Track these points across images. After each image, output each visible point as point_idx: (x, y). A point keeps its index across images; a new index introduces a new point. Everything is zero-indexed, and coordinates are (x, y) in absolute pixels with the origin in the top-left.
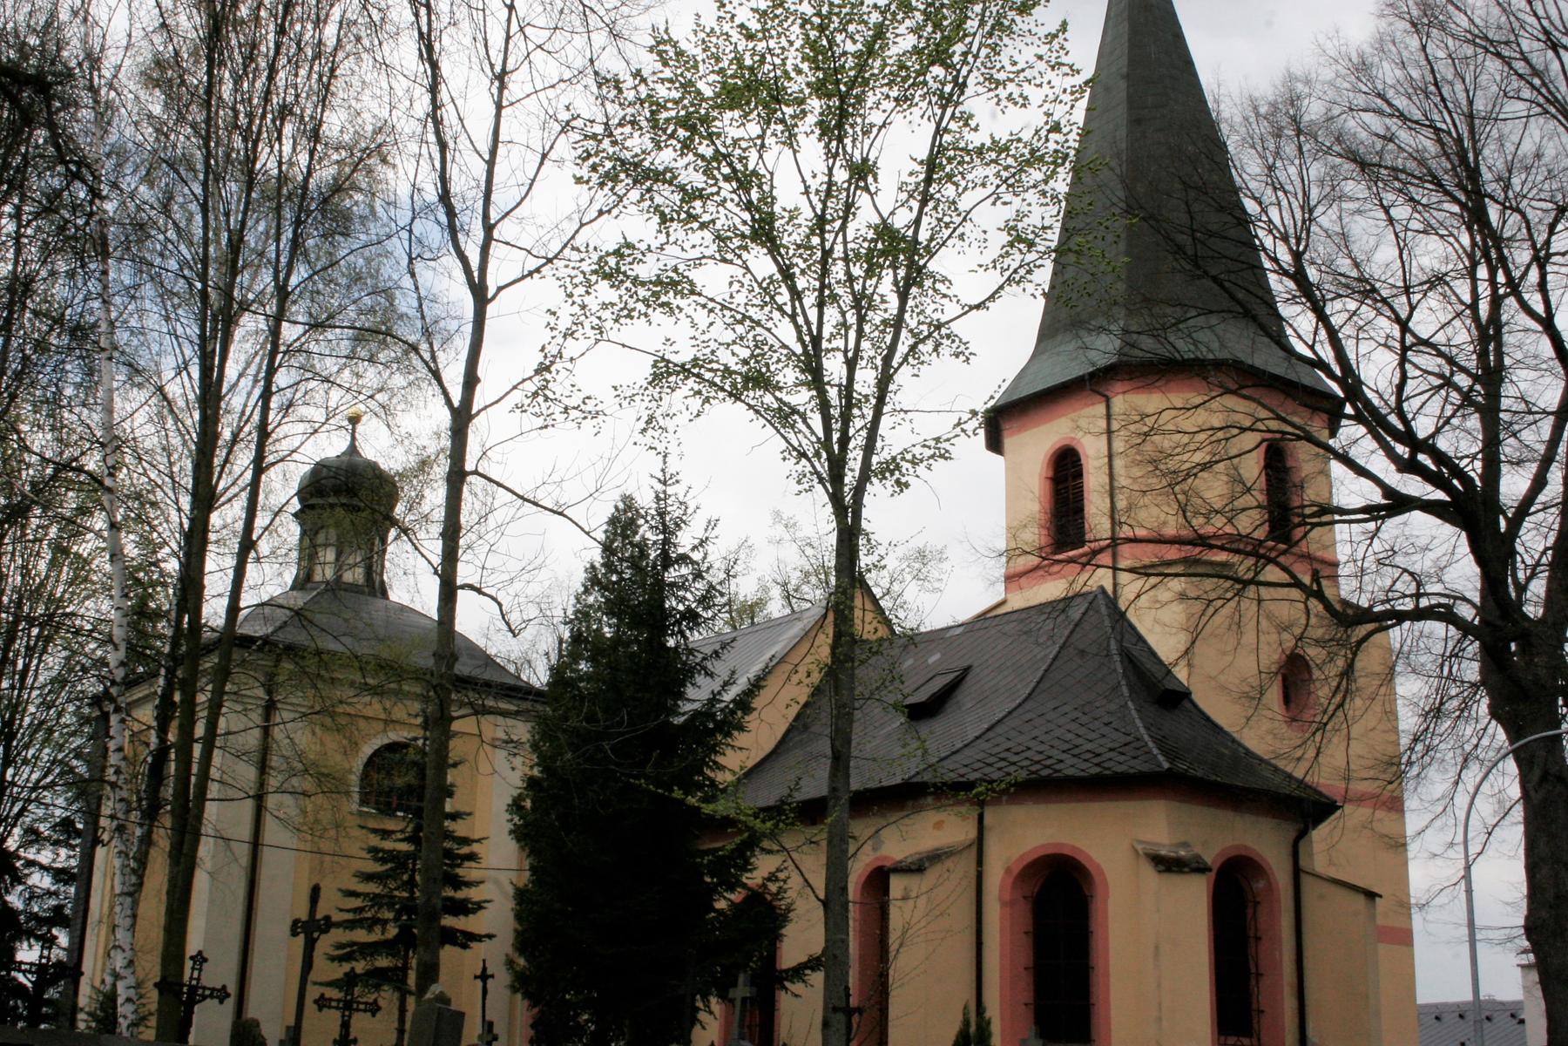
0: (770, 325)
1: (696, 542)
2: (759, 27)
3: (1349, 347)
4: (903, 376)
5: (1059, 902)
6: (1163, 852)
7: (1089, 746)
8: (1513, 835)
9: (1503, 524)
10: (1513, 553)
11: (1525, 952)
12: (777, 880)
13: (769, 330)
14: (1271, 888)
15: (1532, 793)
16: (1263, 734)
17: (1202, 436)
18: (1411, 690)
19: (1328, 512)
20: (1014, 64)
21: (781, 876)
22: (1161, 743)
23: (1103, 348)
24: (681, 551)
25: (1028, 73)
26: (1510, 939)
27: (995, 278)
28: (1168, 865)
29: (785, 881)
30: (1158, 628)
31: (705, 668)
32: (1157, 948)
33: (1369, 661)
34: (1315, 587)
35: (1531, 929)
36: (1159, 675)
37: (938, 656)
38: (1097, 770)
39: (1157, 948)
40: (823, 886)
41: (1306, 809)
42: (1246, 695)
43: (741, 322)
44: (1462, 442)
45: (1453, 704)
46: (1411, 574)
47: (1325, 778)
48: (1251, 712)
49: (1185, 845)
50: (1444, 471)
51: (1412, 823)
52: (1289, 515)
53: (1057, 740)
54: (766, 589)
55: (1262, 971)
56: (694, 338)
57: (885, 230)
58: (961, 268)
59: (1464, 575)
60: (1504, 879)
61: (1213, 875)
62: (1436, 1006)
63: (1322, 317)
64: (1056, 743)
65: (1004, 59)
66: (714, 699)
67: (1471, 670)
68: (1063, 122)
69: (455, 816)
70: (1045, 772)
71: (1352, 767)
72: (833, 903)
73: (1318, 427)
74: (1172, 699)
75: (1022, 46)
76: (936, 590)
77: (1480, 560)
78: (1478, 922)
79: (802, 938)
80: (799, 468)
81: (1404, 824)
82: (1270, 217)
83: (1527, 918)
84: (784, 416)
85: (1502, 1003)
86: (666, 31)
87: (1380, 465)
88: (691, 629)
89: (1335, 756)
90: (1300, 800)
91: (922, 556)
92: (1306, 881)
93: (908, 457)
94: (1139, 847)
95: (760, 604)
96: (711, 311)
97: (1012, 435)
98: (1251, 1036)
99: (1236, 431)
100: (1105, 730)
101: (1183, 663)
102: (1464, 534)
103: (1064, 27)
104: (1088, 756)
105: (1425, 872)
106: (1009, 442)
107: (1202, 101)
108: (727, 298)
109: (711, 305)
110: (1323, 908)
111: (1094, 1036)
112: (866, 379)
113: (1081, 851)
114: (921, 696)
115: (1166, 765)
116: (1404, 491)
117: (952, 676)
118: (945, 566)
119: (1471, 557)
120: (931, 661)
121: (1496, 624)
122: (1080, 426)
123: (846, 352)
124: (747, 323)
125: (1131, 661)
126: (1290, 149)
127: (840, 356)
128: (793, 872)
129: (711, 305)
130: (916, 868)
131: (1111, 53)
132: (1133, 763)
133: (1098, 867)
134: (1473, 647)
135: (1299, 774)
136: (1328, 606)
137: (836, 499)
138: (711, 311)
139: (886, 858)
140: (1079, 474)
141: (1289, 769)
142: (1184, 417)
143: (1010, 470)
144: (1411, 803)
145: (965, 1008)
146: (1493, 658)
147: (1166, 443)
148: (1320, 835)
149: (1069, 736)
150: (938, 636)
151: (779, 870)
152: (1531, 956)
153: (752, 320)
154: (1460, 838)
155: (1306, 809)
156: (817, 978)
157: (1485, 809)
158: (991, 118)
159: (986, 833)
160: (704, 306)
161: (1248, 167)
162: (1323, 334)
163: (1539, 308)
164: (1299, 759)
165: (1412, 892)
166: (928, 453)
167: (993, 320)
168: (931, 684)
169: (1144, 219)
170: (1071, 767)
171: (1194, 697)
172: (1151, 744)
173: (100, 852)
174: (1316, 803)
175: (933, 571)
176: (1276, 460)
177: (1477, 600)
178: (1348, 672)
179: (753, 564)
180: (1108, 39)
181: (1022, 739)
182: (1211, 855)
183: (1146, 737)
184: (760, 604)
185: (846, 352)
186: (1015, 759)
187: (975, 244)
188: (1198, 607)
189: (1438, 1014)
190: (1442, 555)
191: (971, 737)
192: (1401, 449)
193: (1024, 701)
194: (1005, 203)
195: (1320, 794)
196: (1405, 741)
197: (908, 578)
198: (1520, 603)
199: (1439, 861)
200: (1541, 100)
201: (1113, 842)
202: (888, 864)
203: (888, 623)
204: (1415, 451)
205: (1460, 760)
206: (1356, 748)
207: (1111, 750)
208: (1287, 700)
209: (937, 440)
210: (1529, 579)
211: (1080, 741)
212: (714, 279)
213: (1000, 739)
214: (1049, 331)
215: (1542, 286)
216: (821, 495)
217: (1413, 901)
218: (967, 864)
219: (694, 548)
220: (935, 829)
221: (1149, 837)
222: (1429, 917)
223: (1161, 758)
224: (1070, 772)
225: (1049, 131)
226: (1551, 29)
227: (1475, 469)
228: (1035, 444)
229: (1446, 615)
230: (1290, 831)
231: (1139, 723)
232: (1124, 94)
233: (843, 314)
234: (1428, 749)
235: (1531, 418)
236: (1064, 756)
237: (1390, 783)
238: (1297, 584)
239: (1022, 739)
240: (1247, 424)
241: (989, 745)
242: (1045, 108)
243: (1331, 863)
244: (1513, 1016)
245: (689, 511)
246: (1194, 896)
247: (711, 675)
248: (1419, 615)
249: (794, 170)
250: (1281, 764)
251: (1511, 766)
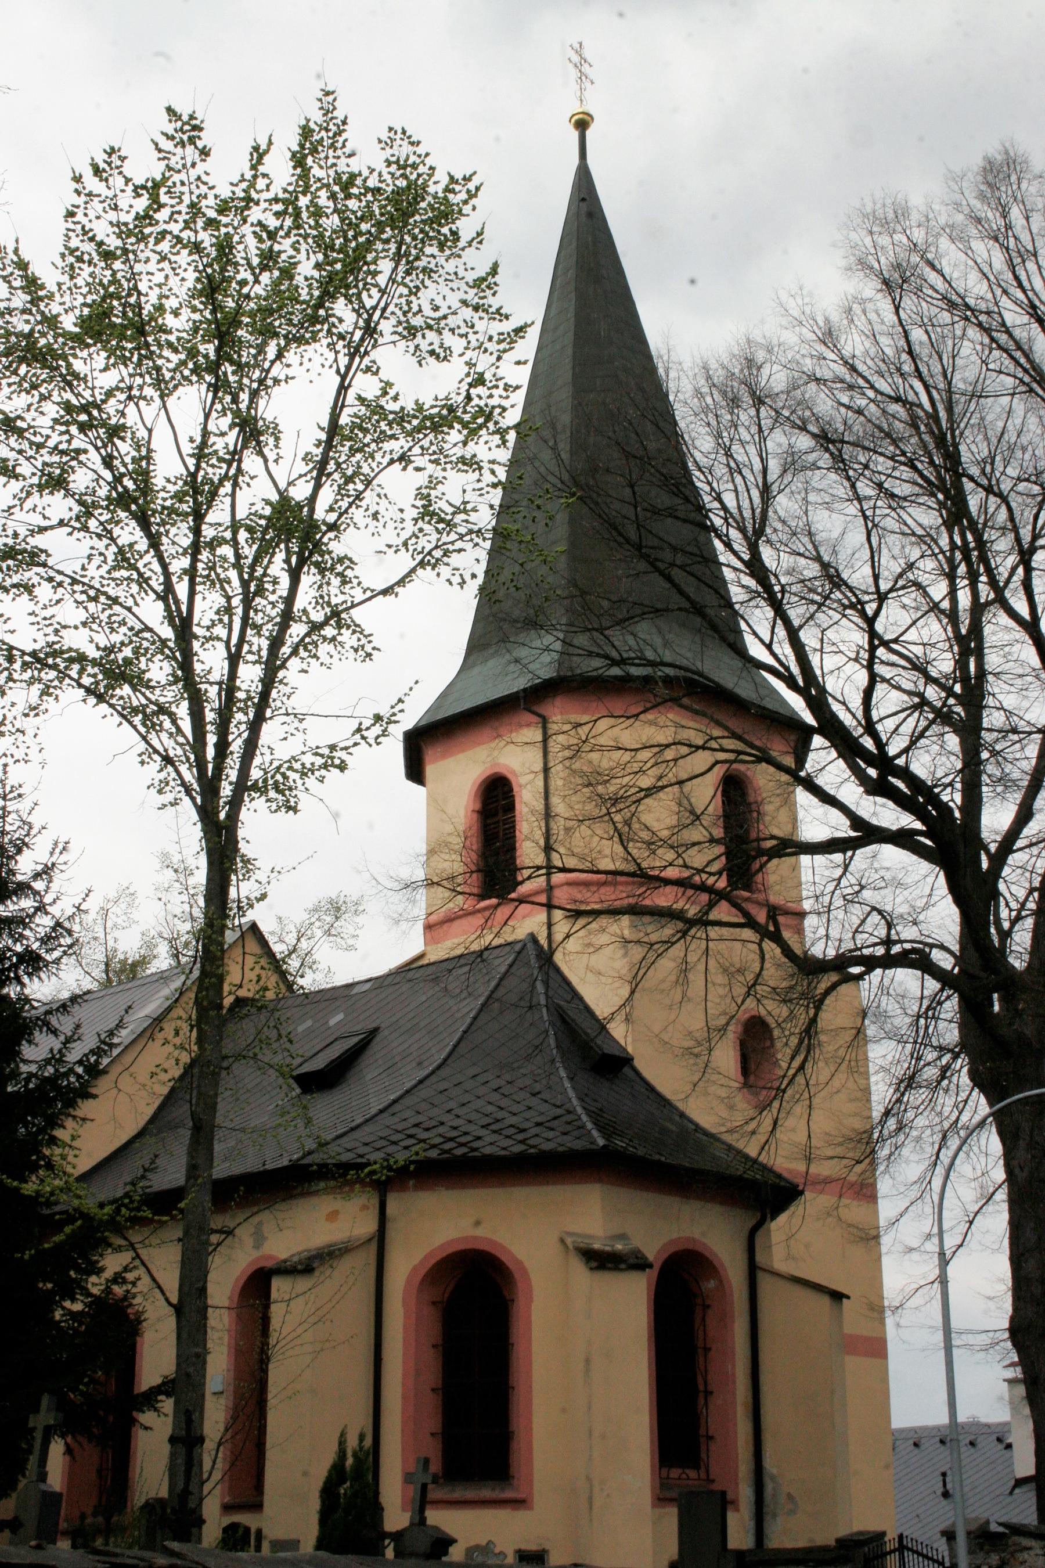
0: (130, 602)
1: (39, 868)
2: (119, 243)
3: (815, 660)
4: (291, 672)
5: (475, 1299)
6: (597, 1246)
7: (513, 1120)
8: (997, 1221)
9: (985, 865)
10: (996, 894)
11: (1012, 1365)
12: (124, 1281)
13: (129, 609)
14: (722, 1285)
15: (1017, 1171)
16: (709, 1100)
17: (645, 755)
18: (884, 1056)
19: (792, 847)
20: (436, 309)
21: (130, 1276)
22: (597, 1117)
23: (539, 657)
24: (19, 878)
25: (452, 321)
26: (994, 1344)
27: (405, 562)
28: (601, 1260)
29: (134, 1284)
30: (590, 977)
31: (47, 1024)
32: (587, 1361)
33: (835, 1014)
34: (772, 928)
35: (1018, 1331)
36: (592, 1033)
37: (340, 1016)
38: (519, 1148)
39: (587, 1361)
40: (177, 1286)
41: (768, 1195)
42: (688, 1052)
43: (95, 599)
44: (936, 761)
45: (931, 1073)
46: (880, 912)
47: (784, 1160)
48: (696, 1078)
49: (622, 1237)
50: (918, 797)
51: (886, 1209)
52: (748, 848)
53: (475, 1116)
54: (150, 945)
55: (710, 1388)
56: (33, 613)
57: (284, 507)
58: (367, 547)
59: (942, 921)
60: (985, 1281)
61: (654, 1273)
62: (914, 1430)
63: (780, 612)
64: (473, 1116)
65: (423, 299)
66: (56, 1059)
67: (950, 1033)
68: (488, 376)
71: (814, 1142)
72: (190, 1309)
73: (781, 750)
74: (612, 1066)
75: (446, 291)
76: (350, 948)
77: (958, 901)
78: (954, 1324)
79: (156, 1357)
80: (163, 775)
81: (876, 1212)
82: (724, 494)
83: (1012, 1319)
84: (149, 717)
85: (988, 1426)
86: (16, 251)
87: (851, 793)
88: (30, 975)
89: (793, 1131)
90: (753, 1184)
91: (336, 909)
92: (765, 1283)
93: (297, 766)
94: (569, 1241)
95: (143, 962)
96: (60, 584)
97: (435, 761)
98: (697, 1467)
99: (685, 750)
100: (533, 1101)
101: (620, 1017)
102: (942, 873)
103: (494, 271)
104: (512, 1131)
105: (901, 1273)
106: (430, 771)
107: (649, 357)
108: (78, 570)
109: (59, 578)
110: (779, 1306)
111: (513, 1471)
112: (250, 675)
113: (504, 1248)
114: (318, 1064)
115: (601, 1142)
116: (874, 821)
117: (356, 1039)
118: (360, 919)
119: (950, 897)
120: (332, 1022)
121: (977, 973)
122: (513, 754)
123: (228, 643)
124: (103, 599)
125: (564, 1021)
126: (745, 416)
127: (221, 646)
128: (147, 1272)
129: (59, 578)
130: (304, 1267)
131: (556, 328)
132: (566, 1139)
133: (520, 1263)
134: (951, 1006)
135: (752, 1151)
136: (787, 951)
137: (207, 813)
138: (60, 584)
139: (270, 1257)
140: (511, 807)
141: (740, 1145)
142: (626, 739)
143: (433, 801)
144: (884, 1186)
145: (343, 1435)
146: (973, 1012)
147: (606, 761)
148: (780, 1226)
149: (490, 1109)
150: (341, 995)
151: (126, 1269)
152: (1019, 1369)
153: (109, 598)
154: (935, 1230)
155: (768, 1195)
156: (167, 1404)
157: (963, 1193)
158: (412, 379)
159: (389, 1226)
160: (50, 579)
161: (701, 444)
162: (781, 632)
163: (1024, 610)
164: (753, 1133)
165: (886, 1293)
166: (319, 761)
167: (415, 629)
168: (328, 1051)
169: (580, 498)
170: (491, 1145)
171: (637, 1063)
172: (584, 1118)
174: (775, 1187)
175: (346, 925)
176: (734, 789)
177: (956, 948)
178: (810, 1028)
179: (135, 915)
180: (553, 312)
181: (434, 1112)
182: (653, 1250)
183: (579, 1110)
184: (143, 962)
185: (228, 643)
186: (424, 1135)
187: (391, 525)
188: (638, 952)
189: (917, 1439)
190: (921, 899)
191: (373, 1111)
192: (872, 772)
193: (439, 1067)
194: (418, 469)
195: (779, 1176)
196: (877, 1112)
197: (319, 933)
198: (1002, 951)
199: (915, 1256)
200: (1027, 379)
201: (536, 1231)
202: (269, 1264)
203: (290, 986)
204: (883, 773)
205: (938, 1138)
206: (821, 1123)
207: (538, 1124)
208: (745, 1070)
209: (333, 748)
210: (1013, 923)
211: (500, 1115)
212: (67, 550)
213: (408, 1113)
214: (479, 645)
215: (1027, 586)
216: (188, 812)
217: (886, 1303)
218: (363, 1262)
219: (37, 876)
220: (328, 1220)
222: (903, 1322)
223: (595, 1133)
224: (488, 1150)
225: (470, 385)
226: (1038, 303)
227: (953, 798)
228: (461, 772)
229: (918, 959)
230: (740, 1221)
231: (571, 1094)
232: (569, 376)
233: (229, 599)
234: (900, 1128)
235: (1016, 737)
236: (482, 1132)
237: (858, 1162)
238: (751, 923)
239: (434, 1112)
240: (700, 743)
241: (396, 1119)
242: (466, 358)
243: (789, 1257)
244: (999, 1440)
245: (33, 832)
246: (631, 1300)
247: (55, 1032)
248: (888, 962)
249: (174, 426)
250: (728, 1138)
251: (992, 1142)
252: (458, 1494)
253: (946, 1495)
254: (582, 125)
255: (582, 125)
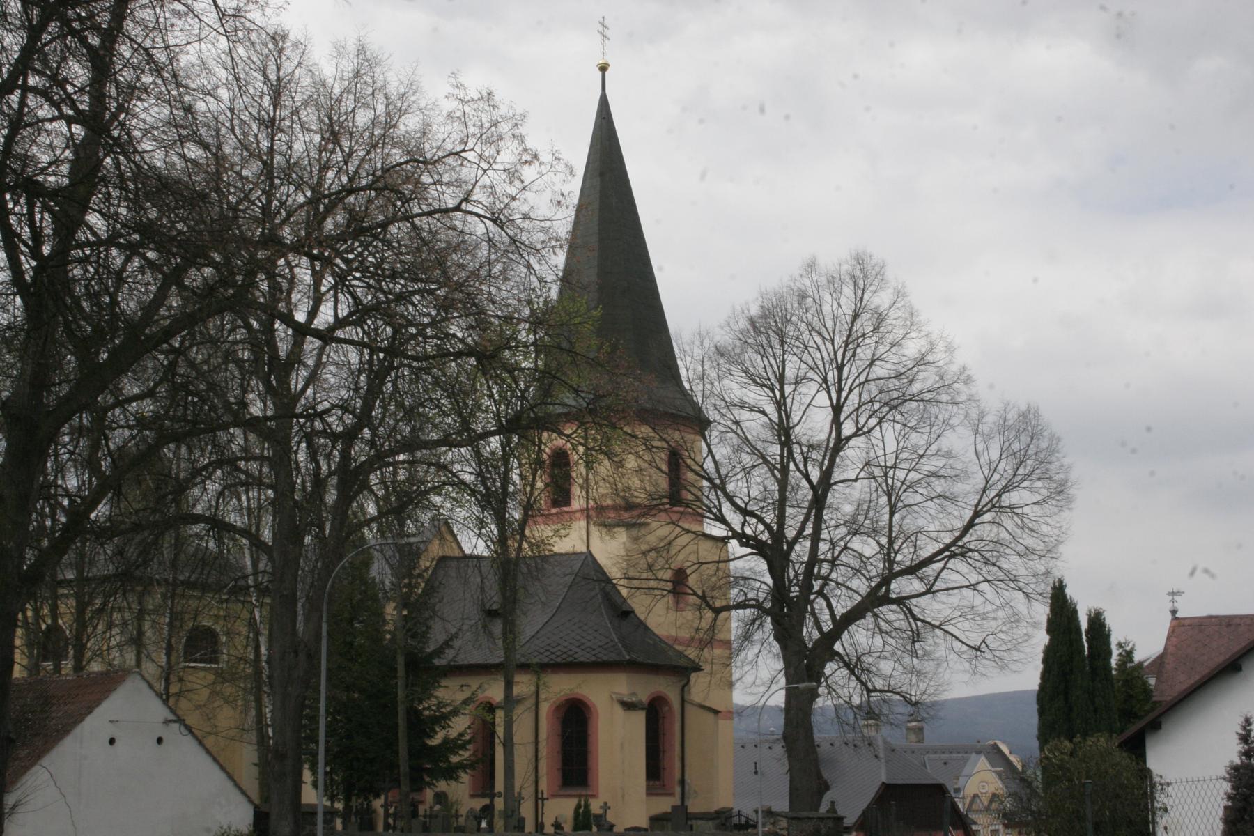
5: (575, 720)
7: (589, 644)
28: (628, 706)
38: (593, 659)
41: (683, 671)
69: (439, 652)
70: (570, 659)
170: (582, 657)
173: (707, 531)
182: (644, 697)
201: (604, 694)
221: (617, 690)
224: (582, 659)
246: (638, 720)
252: (569, 792)
253: (756, 773)
254: (603, 69)
255: (603, 69)
